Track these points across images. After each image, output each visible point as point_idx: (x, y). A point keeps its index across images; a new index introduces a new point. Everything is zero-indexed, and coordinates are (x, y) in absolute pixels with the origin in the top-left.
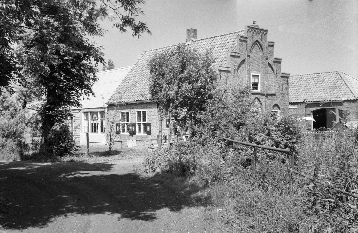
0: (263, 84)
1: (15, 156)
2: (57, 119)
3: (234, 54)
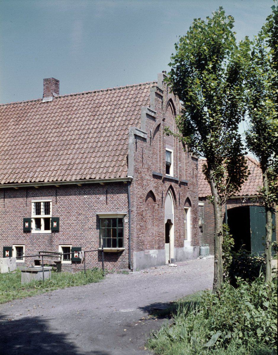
0: (176, 165)
2: (276, 39)
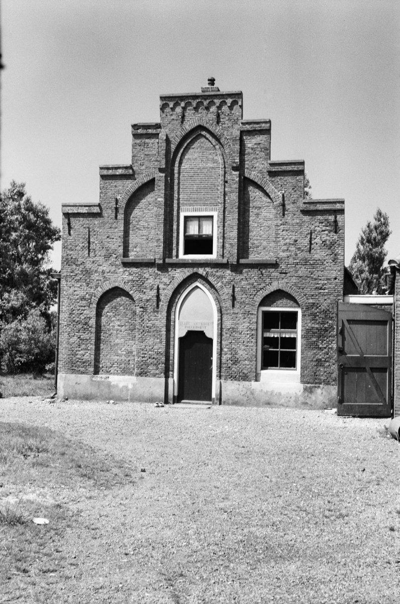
1: (313, 398)
3: (110, 172)
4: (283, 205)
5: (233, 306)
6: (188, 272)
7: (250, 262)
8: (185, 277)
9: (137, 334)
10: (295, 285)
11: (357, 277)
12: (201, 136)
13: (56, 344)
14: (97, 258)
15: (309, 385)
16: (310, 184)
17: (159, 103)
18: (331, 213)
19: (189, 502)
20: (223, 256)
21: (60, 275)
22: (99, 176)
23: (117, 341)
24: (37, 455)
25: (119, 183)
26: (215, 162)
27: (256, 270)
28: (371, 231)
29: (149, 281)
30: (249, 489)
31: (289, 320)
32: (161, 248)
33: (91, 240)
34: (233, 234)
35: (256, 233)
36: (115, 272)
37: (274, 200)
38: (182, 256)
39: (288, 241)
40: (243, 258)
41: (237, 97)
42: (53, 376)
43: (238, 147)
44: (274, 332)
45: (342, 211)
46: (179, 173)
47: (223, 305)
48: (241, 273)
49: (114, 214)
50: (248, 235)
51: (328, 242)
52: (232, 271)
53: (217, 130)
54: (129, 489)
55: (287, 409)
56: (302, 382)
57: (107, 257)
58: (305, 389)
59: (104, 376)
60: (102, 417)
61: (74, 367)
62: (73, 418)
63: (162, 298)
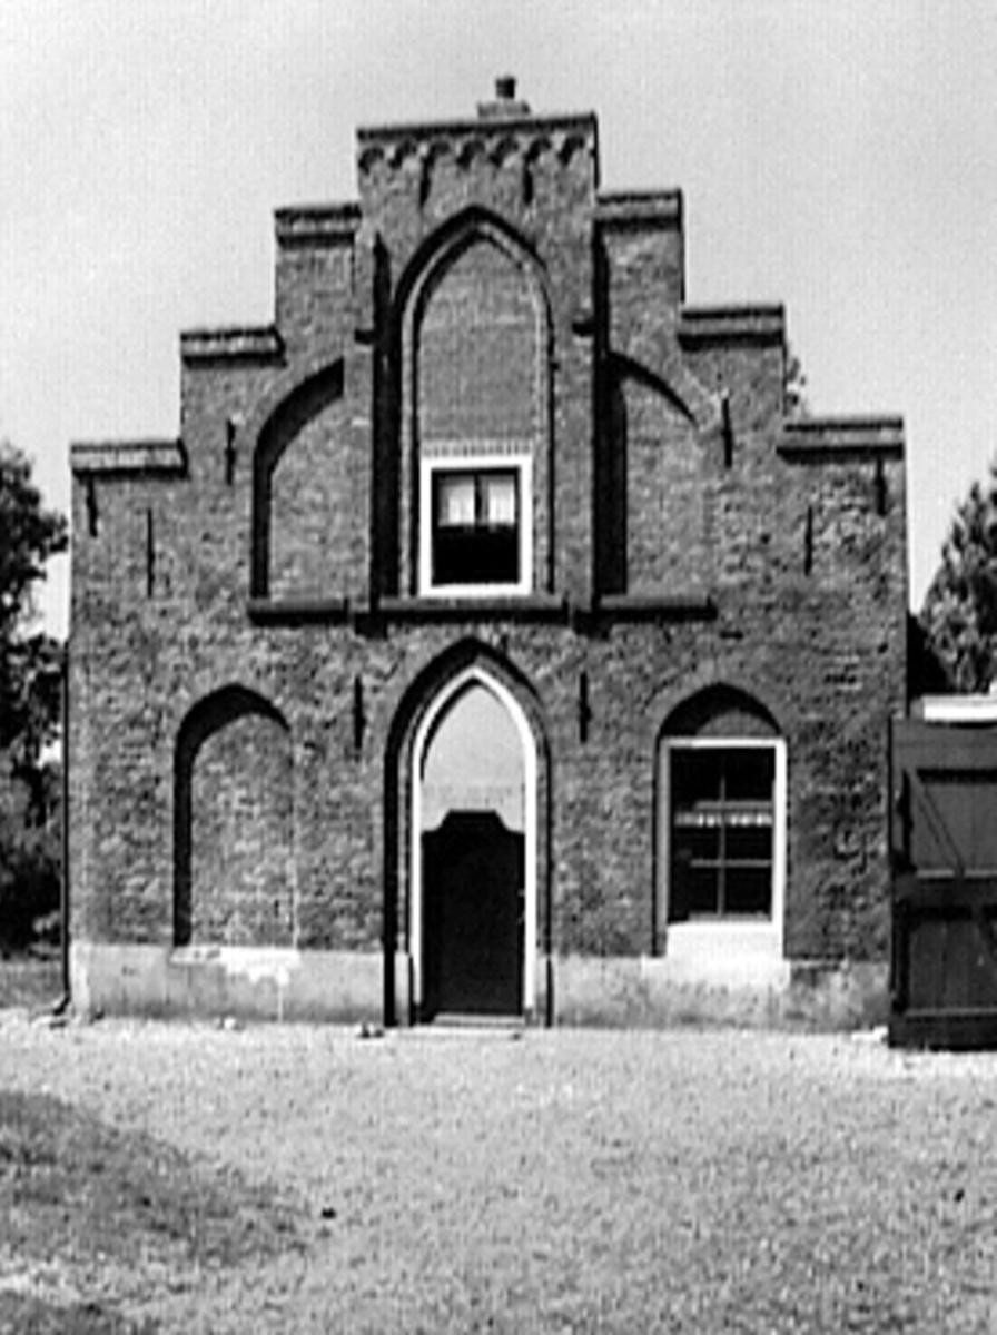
4: (726, 433)
5: (584, 736)
6: (446, 636)
7: (632, 604)
8: (438, 649)
9: (297, 826)
10: (767, 667)
11: (945, 644)
12: (481, 237)
13: (60, 855)
14: (175, 602)
15: (807, 964)
16: (803, 371)
17: (354, 148)
18: (868, 454)
19: (463, 1298)
20: (551, 587)
21: (66, 655)
22: (177, 360)
23: (240, 846)
24: (23, 1169)
25: (239, 377)
26: (518, 308)
27: (649, 628)
28: (981, 509)
29: (331, 666)
30: (633, 1260)
31: (751, 775)
32: (365, 569)
33: (158, 547)
34: (580, 520)
35: (648, 517)
36: (227, 642)
37: (698, 418)
38: (427, 589)
39: (742, 539)
40: (612, 591)
41: (582, 127)
42: (58, 951)
43: (586, 266)
44: (706, 812)
45: (897, 451)
46: (416, 345)
47: (554, 732)
48: (605, 637)
49: (221, 472)
50: (624, 525)
51: (859, 543)
52: (578, 631)
53: (527, 219)
54: (287, 1265)
55: (745, 1034)
56: (788, 954)
57: (204, 597)
58: (797, 975)
59: (204, 949)
60: (203, 1064)
61: (115, 925)
62: (118, 1068)
63: (370, 716)
